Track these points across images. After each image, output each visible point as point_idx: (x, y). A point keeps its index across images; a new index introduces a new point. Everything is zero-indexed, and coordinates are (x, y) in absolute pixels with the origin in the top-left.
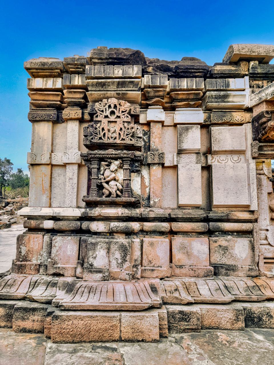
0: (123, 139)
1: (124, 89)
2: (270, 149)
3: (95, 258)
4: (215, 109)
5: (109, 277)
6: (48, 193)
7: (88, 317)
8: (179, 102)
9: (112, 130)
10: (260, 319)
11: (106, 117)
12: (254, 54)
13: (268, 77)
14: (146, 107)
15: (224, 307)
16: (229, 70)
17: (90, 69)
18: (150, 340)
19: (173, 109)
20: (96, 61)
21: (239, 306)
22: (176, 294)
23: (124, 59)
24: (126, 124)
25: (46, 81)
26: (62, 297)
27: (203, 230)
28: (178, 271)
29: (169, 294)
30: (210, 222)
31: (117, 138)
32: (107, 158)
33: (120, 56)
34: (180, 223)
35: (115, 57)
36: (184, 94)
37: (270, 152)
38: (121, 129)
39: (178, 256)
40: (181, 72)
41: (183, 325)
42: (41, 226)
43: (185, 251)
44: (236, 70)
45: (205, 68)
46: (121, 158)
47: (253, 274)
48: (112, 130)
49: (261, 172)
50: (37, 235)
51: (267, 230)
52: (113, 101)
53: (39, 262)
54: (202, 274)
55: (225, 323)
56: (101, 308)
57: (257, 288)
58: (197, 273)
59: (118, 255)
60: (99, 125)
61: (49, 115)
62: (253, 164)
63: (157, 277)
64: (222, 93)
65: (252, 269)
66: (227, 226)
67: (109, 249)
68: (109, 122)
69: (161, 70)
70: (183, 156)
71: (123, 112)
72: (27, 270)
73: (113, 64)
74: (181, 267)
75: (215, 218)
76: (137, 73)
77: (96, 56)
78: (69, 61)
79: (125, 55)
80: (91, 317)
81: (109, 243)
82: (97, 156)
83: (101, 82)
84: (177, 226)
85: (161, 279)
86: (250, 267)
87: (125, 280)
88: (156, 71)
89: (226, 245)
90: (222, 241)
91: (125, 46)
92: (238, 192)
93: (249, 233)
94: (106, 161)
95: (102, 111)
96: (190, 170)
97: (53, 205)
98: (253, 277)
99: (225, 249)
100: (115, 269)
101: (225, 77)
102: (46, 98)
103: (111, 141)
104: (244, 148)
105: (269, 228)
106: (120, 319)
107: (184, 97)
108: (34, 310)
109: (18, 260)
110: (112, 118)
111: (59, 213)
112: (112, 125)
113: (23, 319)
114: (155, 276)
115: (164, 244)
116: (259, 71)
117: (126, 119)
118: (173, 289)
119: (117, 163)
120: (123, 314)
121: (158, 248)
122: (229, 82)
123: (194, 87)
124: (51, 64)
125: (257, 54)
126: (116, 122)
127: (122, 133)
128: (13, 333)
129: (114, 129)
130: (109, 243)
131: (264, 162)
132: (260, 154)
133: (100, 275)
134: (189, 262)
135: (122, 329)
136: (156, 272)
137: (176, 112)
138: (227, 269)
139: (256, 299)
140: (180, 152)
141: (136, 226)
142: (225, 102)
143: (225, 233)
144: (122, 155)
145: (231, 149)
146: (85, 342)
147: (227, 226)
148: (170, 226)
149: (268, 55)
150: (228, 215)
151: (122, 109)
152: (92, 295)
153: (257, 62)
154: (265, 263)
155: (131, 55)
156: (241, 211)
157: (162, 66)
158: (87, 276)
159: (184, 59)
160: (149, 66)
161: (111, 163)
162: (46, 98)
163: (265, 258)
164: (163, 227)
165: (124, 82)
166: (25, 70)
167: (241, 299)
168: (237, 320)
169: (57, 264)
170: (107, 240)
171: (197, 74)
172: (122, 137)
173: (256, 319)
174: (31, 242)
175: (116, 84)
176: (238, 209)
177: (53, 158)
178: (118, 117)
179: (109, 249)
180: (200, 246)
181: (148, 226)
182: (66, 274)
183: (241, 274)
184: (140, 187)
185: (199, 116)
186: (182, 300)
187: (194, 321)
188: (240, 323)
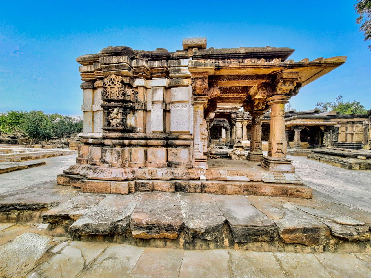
0: (118, 97)
1: (119, 69)
2: (201, 99)
3: (106, 157)
4: (175, 77)
5: (111, 166)
6: (92, 125)
7: (96, 182)
8: (154, 74)
9: (113, 92)
10: (185, 188)
11: (110, 85)
12: (194, 44)
13: (204, 57)
14: (135, 78)
15: (165, 182)
16: (182, 54)
17: (102, 60)
18: (123, 193)
19: (150, 79)
20: (106, 54)
21: (174, 181)
22: (144, 175)
23: (119, 53)
24: (119, 88)
25: (87, 68)
26: (90, 174)
27: (163, 144)
28: (149, 164)
29: (140, 175)
30: (168, 140)
31: (115, 96)
32: (111, 107)
33: (116, 51)
34: (152, 141)
35: (114, 51)
36: (155, 70)
37: (200, 101)
38: (117, 92)
39: (150, 157)
40: (154, 57)
41: (143, 189)
42: (88, 142)
43: (154, 155)
44: (186, 54)
45: (166, 54)
46: (118, 107)
47: (189, 167)
48: (113, 92)
49: (197, 113)
50: (87, 146)
51: (199, 144)
52: (113, 76)
53: (88, 158)
54: (161, 166)
55: (165, 189)
56: (103, 179)
57: (188, 174)
58: (158, 166)
59: (116, 156)
60: (106, 89)
61: (89, 86)
62: (192, 107)
63: (137, 167)
64: (176, 68)
65: (188, 164)
66: (177, 142)
67: (112, 153)
68: (111, 88)
69: (144, 57)
70: (155, 105)
71: (117, 82)
72: (82, 162)
73: (113, 56)
74: (151, 162)
75: (171, 138)
76: (124, 60)
77: (104, 52)
78: (95, 56)
79: (119, 50)
80: (98, 182)
81: (112, 150)
82: (106, 106)
83: (107, 66)
84: (150, 142)
85: (140, 168)
86: (188, 163)
87: (119, 167)
88: (141, 57)
89: (176, 152)
90: (174, 150)
91: (119, 44)
92: (183, 124)
93: (188, 146)
94: (111, 109)
95: (108, 82)
96: (157, 113)
97: (96, 131)
98: (189, 168)
99: (176, 154)
100: (114, 162)
101: (178, 59)
102: (89, 76)
103: (112, 98)
104: (187, 100)
105: (199, 143)
106: (110, 184)
107: (156, 72)
108: (79, 179)
109: (79, 157)
110: (112, 86)
111: (93, 135)
112: (113, 89)
113: (75, 183)
114: (137, 166)
115: (142, 151)
116: (198, 54)
117: (119, 86)
118: (143, 172)
119: (116, 109)
120: (112, 182)
121: (138, 153)
122: (180, 62)
123: (161, 66)
124: (88, 58)
125: (195, 44)
126: (114, 87)
127: (117, 94)
128: (71, 188)
129: (115, 91)
130: (112, 150)
131: (199, 107)
132: (195, 103)
133: (108, 165)
134: (156, 160)
135: (111, 188)
136: (137, 164)
137: (152, 80)
138: (175, 164)
139: (185, 179)
140: (153, 103)
141: (126, 142)
142: (179, 73)
143: (178, 146)
144: (118, 105)
145: (181, 100)
146: (96, 193)
147: (177, 142)
148: (146, 142)
149: (202, 44)
150: (178, 136)
151: (117, 80)
152: (102, 173)
153: (197, 49)
154: (195, 161)
155: (122, 50)
156: (186, 134)
157: (145, 54)
158: (102, 165)
159: (157, 49)
160: (136, 55)
161: (113, 109)
162: (89, 76)
163: (195, 159)
164: (141, 142)
165: (118, 66)
166: (77, 62)
167: (178, 178)
168: (171, 187)
169: (94, 159)
170: (111, 148)
171: (163, 58)
172: (117, 95)
173: (183, 188)
174: (84, 149)
175: (115, 67)
176: (185, 133)
177: (93, 108)
178: (115, 85)
179: (112, 153)
180: (161, 152)
181: (134, 142)
182: (97, 164)
183: (182, 167)
184: (134, 122)
185: (164, 82)
186: (145, 178)
187: (148, 187)
188: (172, 189)
